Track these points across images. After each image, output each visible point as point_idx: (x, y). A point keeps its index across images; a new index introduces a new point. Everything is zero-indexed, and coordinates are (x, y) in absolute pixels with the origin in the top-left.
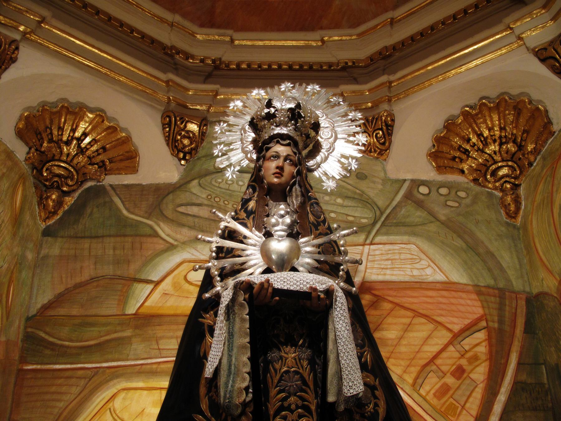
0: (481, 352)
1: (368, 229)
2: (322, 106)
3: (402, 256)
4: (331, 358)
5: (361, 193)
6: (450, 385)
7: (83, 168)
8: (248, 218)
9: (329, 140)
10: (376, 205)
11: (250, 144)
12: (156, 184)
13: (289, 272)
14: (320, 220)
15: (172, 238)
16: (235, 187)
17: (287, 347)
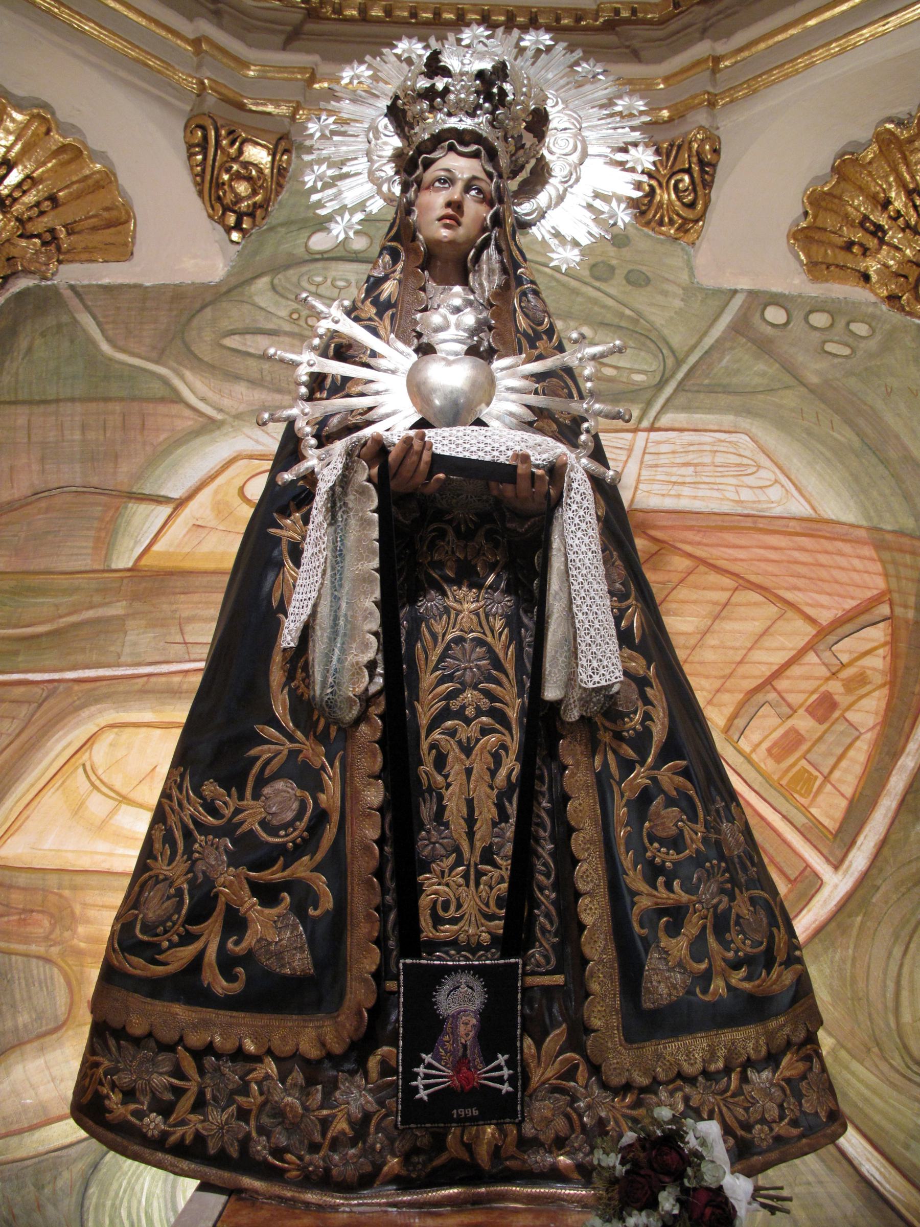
0: (875, 669)
1: (647, 395)
2: (557, 81)
3: (719, 459)
5: (635, 316)
6: (803, 732)
7: (7, 245)
8: (381, 318)
10: (667, 344)
12: (175, 285)
14: (540, 328)
15: (211, 406)
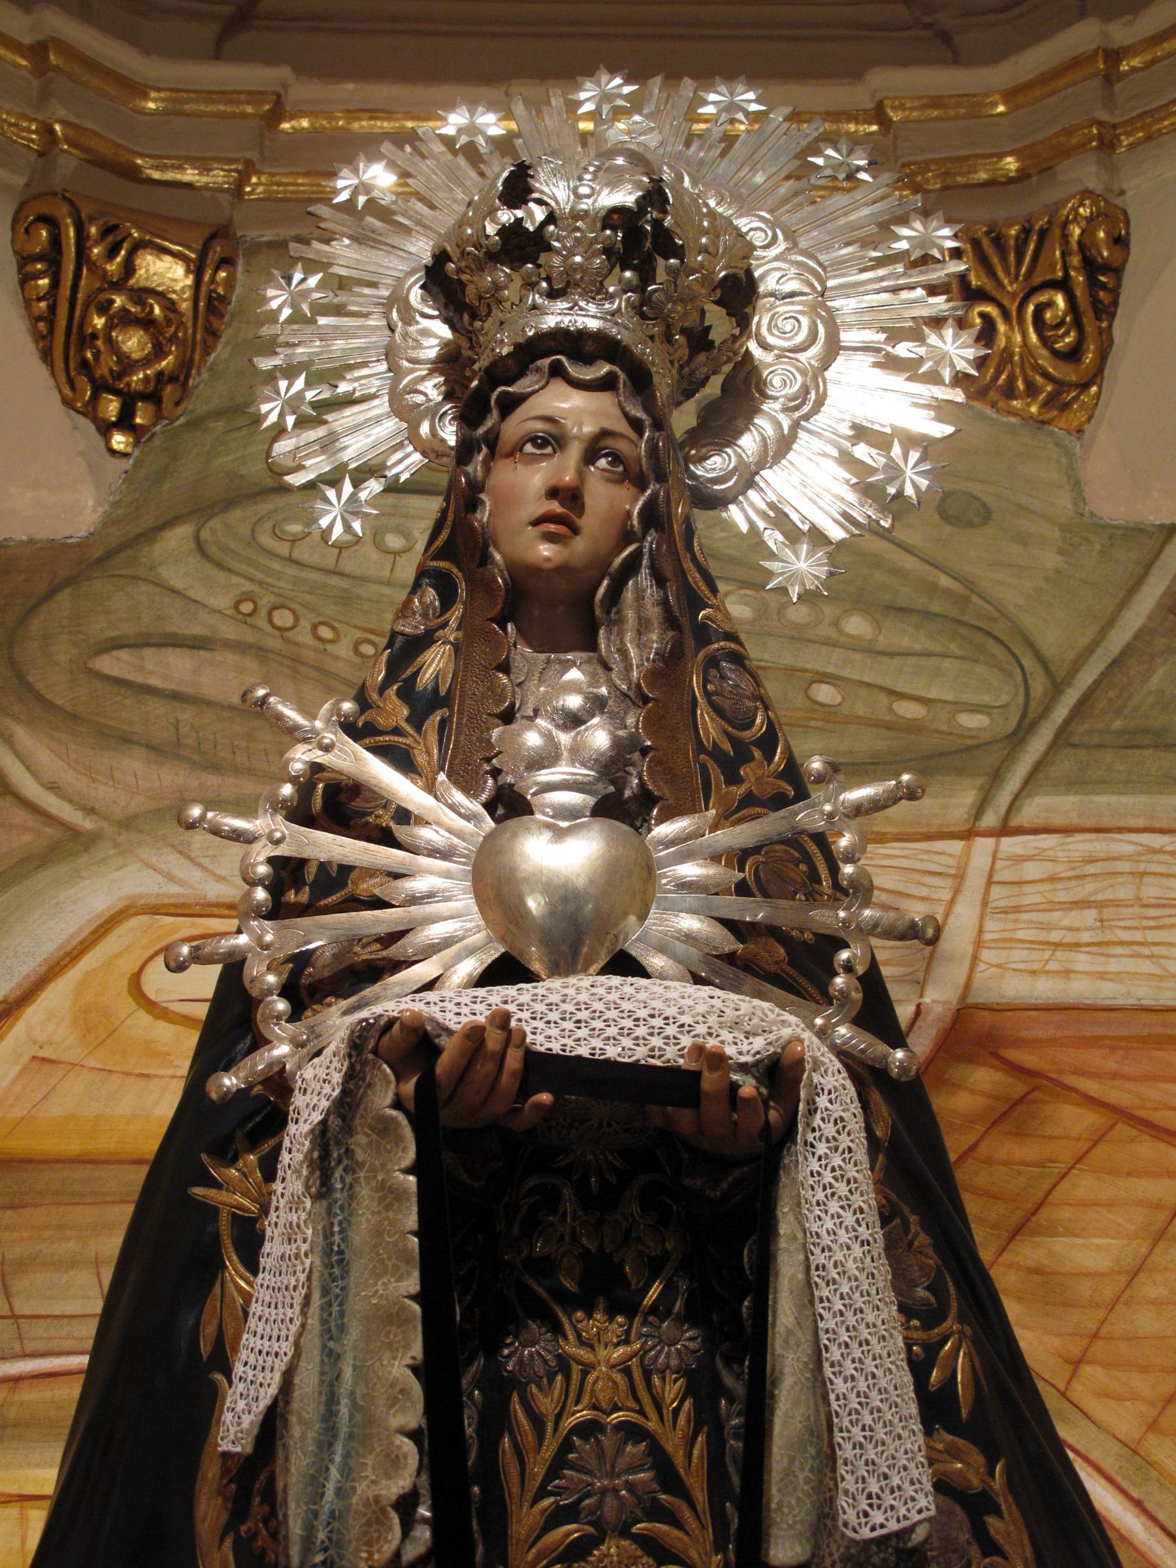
1: (991, 759)
4: (787, 1370)
8: (418, 728)
9: (798, 356)
11: (431, 372)
13: (602, 979)
14: (747, 735)
15: (71, 801)
16: (369, 561)
17: (590, 1316)
